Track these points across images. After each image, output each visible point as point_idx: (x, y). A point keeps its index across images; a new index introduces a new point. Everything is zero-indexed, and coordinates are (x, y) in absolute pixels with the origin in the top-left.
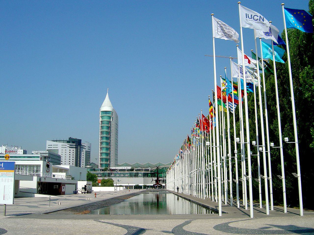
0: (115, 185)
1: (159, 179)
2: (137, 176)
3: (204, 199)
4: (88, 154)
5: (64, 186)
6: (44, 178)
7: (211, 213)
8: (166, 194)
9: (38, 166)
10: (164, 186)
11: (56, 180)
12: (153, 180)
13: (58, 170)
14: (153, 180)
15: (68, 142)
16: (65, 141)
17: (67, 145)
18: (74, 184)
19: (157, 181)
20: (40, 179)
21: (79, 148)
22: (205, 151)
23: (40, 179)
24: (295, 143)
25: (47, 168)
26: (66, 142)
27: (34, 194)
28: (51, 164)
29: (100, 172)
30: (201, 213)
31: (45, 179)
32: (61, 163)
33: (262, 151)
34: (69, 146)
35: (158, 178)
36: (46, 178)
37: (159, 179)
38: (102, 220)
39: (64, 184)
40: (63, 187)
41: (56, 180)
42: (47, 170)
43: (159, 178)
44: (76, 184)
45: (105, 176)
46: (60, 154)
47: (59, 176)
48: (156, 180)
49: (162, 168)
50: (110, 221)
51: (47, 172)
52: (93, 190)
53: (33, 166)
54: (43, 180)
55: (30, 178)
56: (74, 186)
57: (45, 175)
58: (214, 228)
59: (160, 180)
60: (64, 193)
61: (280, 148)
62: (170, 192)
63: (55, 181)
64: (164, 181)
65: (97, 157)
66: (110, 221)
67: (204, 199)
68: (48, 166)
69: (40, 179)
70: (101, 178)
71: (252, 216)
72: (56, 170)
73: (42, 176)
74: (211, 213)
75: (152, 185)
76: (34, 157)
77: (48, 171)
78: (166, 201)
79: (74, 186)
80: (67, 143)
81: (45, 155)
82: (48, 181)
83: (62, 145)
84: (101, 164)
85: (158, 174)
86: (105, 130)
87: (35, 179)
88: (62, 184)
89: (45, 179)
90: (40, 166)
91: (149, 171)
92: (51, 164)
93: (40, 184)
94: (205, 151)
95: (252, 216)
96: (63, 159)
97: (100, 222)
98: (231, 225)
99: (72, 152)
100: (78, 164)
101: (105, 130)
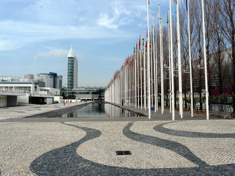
0: (76, 98)
2: (89, 94)
4: (61, 82)
7: (137, 116)
8: (104, 103)
9: (30, 87)
15: (49, 75)
17: (49, 76)
19: (100, 97)
20: (31, 95)
21: (55, 78)
23: (31, 95)
24: (178, 77)
28: (38, 86)
29: (67, 91)
30: (129, 116)
38: (69, 123)
39: (46, 98)
45: (71, 94)
46: (44, 81)
50: (72, 123)
53: (27, 87)
54: (32, 96)
58: (154, 128)
60: (46, 103)
62: (107, 103)
64: (104, 97)
65: (65, 83)
66: (72, 123)
68: (36, 87)
70: (68, 95)
71: (150, 117)
72: (41, 90)
74: (137, 116)
78: (104, 107)
82: (35, 96)
84: (68, 87)
85: (100, 92)
86: (70, 71)
90: (30, 87)
92: (38, 86)
95: (150, 117)
96: (46, 84)
97: (64, 124)
98: (164, 126)
99: (51, 80)
100: (55, 87)
101: (19, 88)
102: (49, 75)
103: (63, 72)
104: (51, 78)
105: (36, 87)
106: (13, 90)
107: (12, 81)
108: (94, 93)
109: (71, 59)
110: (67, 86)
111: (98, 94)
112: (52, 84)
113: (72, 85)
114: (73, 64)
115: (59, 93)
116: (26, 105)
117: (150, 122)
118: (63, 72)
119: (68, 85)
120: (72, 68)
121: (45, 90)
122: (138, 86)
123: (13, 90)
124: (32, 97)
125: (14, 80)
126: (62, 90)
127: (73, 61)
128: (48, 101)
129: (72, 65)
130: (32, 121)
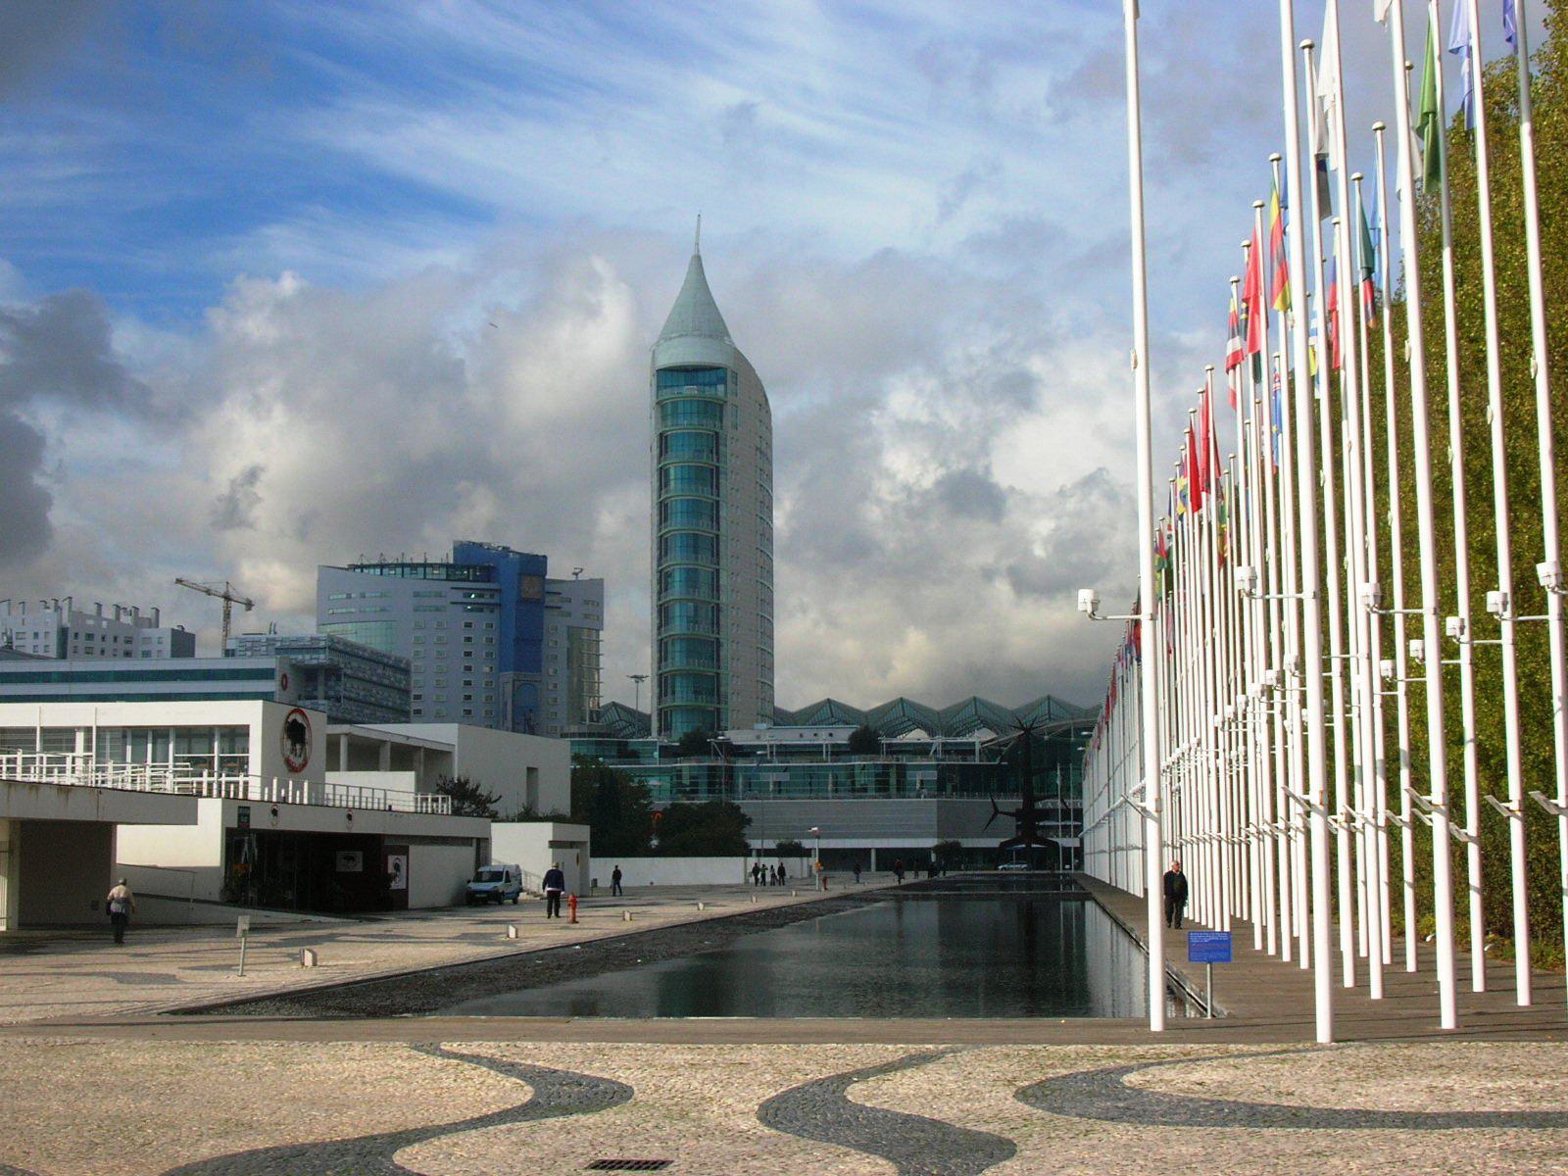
1: (1040, 805)
3: (1376, 992)
5: (403, 858)
6: (269, 811)
9: (236, 735)
10: (1067, 850)
11: (349, 817)
12: (997, 812)
13: (386, 754)
14: (997, 812)
16: (388, 566)
17: (450, 592)
18: (465, 841)
19: (1029, 820)
20: (244, 813)
22: (1473, 408)
25: (288, 744)
26: (443, 571)
27: (563, 839)
31: (275, 812)
32: (414, 706)
33: (1423, 659)
34: (459, 596)
35: (1030, 800)
36: (281, 808)
37: (1040, 805)
39: (402, 844)
40: (392, 859)
41: (349, 817)
42: (292, 757)
43: (1040, 799)
44: (478, 840)
47: (366, 793)
48: (1018, 815)
49: (1060, 735)
51: (293, 769)
52: (595, 881)
53: (205, 734)
54: (260, 821)
55: (180, 809)
56: (469, 852)
57: (279, 792)
59: (1047, 814)
61: (1500, 646)
63: (340, 827)
65: (627, 665)
67: (1376, 992)
69: (239, 816)
72: (366, 756)
73: (257, 797)
75: (994, 843)
76: (45, 677)
77: (297, 761)
79: (469, 852)
80: (447, 580)
81: (308, 659)
83: (417, 595)
87: (211, 813)
88: (387, 843)
89: (275, 812)
91: (973, 752)
93: (235, 839)
94: (1473, 408)
102: (451, 571)
103: (611, 544)
104: (473, 617)
105: (296, 732)
106: (79, 763)
107: (63, 655)
108: (963, 777)
109: (689, 390)
110: (646, 701)
111: (1003, 789)
112: (103, 609)
113: (708, 686)
114: (714, 443)
115: (557, 792)
116: (200, 913)
117: (1446, 1048)
118: (611, 544)
119: (664, 684)
120: (704, 527)
121: (402, 757)
122: (1465, 652)
123: (79, 763)
124: (264, 836)
125: (82, 643)
126: (611, 735)
127: (713, 409)
128: (427, 872)
129: (706, 495)
130: (1293, 353)
